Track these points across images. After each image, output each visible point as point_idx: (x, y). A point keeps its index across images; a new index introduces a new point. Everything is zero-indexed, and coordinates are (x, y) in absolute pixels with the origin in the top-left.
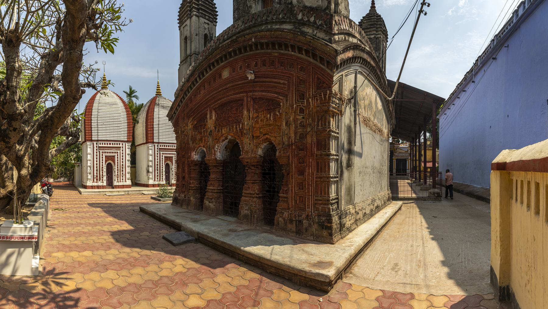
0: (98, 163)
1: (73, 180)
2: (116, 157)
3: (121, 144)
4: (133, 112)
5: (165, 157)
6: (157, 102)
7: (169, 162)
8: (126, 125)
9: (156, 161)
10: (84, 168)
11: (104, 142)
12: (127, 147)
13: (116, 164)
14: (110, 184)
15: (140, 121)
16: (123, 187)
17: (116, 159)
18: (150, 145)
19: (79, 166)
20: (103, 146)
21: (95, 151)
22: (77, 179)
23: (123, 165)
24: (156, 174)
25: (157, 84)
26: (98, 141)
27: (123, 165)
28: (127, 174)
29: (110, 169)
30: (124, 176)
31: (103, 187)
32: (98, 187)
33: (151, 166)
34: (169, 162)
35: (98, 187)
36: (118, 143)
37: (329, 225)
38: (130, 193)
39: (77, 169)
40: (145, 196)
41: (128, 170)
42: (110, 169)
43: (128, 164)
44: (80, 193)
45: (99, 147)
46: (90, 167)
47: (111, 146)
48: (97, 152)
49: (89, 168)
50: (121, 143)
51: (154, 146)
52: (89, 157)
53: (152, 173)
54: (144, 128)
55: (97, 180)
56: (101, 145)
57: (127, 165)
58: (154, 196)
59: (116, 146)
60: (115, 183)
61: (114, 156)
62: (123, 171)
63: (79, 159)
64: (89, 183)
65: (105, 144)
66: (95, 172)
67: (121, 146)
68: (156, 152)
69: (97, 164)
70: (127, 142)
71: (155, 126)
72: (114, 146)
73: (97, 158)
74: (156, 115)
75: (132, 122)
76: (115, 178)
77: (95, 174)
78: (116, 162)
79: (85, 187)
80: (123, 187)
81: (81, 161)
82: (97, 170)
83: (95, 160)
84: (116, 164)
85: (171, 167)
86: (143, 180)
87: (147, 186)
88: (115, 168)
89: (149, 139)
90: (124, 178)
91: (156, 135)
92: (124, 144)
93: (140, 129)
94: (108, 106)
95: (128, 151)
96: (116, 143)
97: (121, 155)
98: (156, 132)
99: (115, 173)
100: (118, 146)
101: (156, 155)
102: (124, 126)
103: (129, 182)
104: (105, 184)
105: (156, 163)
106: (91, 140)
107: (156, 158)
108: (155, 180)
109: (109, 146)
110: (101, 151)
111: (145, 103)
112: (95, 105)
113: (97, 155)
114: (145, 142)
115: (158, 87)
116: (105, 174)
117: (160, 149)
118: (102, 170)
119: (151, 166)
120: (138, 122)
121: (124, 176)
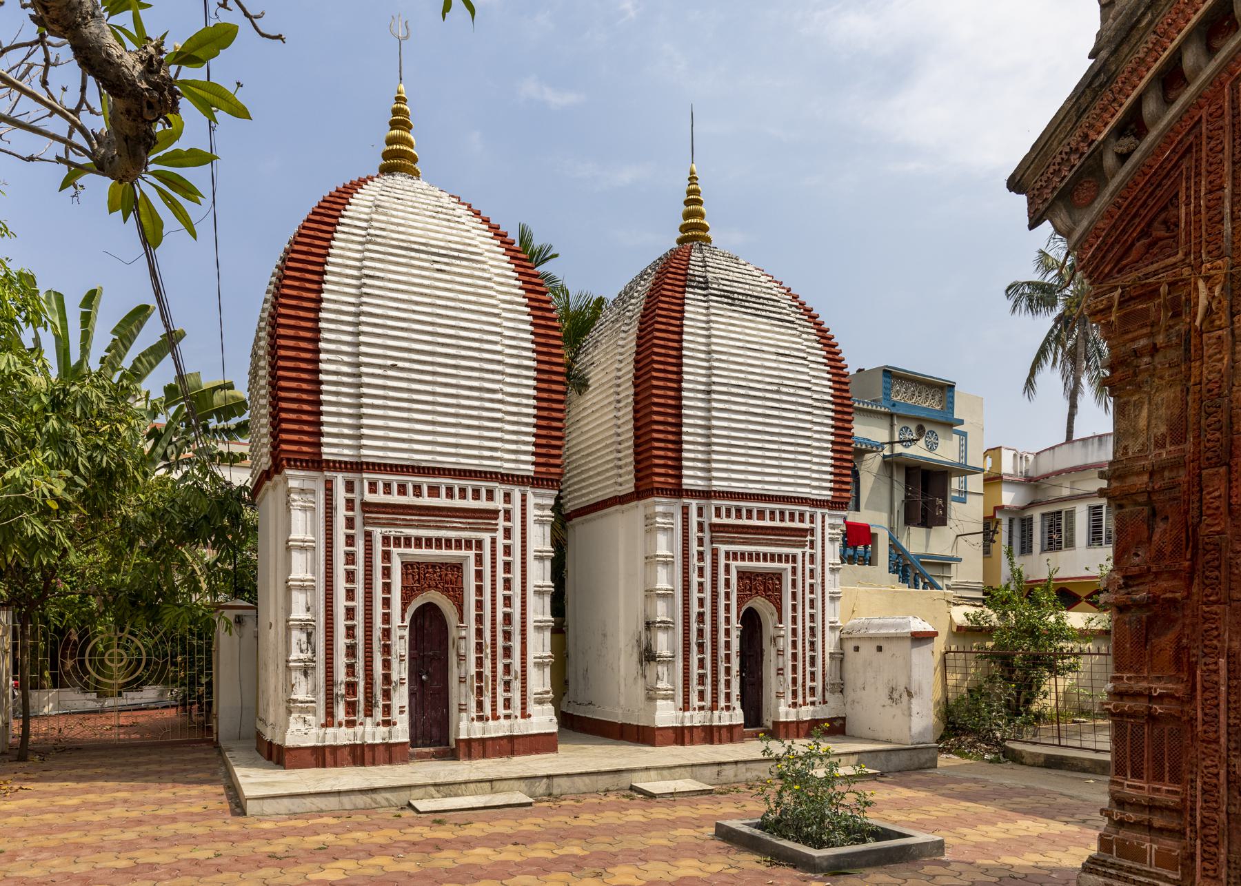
0: (359, 603)
1: (207, 707)
2: (471, 568)
3: (507, 497)
4: (562, 333)
5: (742, 575)
6: (695, 270)
7: (760, 604)
8: (527, 386)
9: (695, 595)
10: (272, 638)
11: (395, 479)
12: (532, 512)
13: (472, 612)
14: (433, 733)
15: (596, 377)
16: (511, 745)
17: (470, 583)
18: (660, 505)
19: (239, 620)
20: (394, 498)
21: (340, 530)
22: (227, 698)
23: (508, 618)
24: (695, 671)
25: (684, 185)
26: (358, 466)
27: (508, 618)
28: (532, 672)
29: (430, 635)
30: (516, 685)
31: (389, 753)
32: (360, 755)
33: (667, 626)
34: (760, 604)
35: (360, 755)
36: (483, 485)
37: (802, 733)
38: (561, 785)
39: (226, 643)
40: (659, 812)
41: (540, 645)
42: (430, 635)
43: (540, 611)
44: (237, 804)
45: (367, 507)
46: (307, 628)
47: (442, 501)
48: (350, 540)
49: (298, 636)
50: (500, 490)
51: (685, 510)
52: (301, 568)
53: (670, 662)
54: (627, 413)
55: (351, 708)
56: (380, 498)
57: (532, 617)
58: (735, 824)
59: (469, 503)
60: (466, 727)
61: (458, 567)
62: (507, 652)
63: (243, 584)
64: (301, 732)
65: (402, 490)
66: (341, 660)
67: (498, 503)
68: (694, 548)
69: (350, 613)
70: (535, 481)
71: (692, 401)
72: (457, 503)
73: (350, 576)
74: (692, 339)
75: (559, 381)
76: (460, 694)
77: (341, 675)
78: (471, 598)
79: (276, 756)
80: (511, 745)
81: (254, 599)
82: (351, 651)
83: (341, 584)
84: (472, 612)
85: (453, 633)
86: (621, 703)
87: (644, 735)
88: (464, 637)
89: (656, 461)
90: (516, 696)
91: (691, 452)
92: (517, 493)
93: (603, 417)
94: (422, 260)
95: (540, 540)
96: (470, 484)
97: (501, 558)
98: (691, 434)
99: (464, 665)
100: (483, 504)
101: (694, 561)
102: (518, 389)
103: (543, 720)
104: (401, 732)
105: (695, 609)
106: (316, 463)
107: (695, 579)
108: (686, 706)
109: (426, 500)
110: (378, 533)
111: (611, 295)
112: (344, 250)
113: (350, 558)
114: (629, 488)
115: (693, 198)
116: (400, 671)
117: (714, 527)
118: (387, 649)
119: (667, 626)
120: (582, 385)
121: (516, 685)
